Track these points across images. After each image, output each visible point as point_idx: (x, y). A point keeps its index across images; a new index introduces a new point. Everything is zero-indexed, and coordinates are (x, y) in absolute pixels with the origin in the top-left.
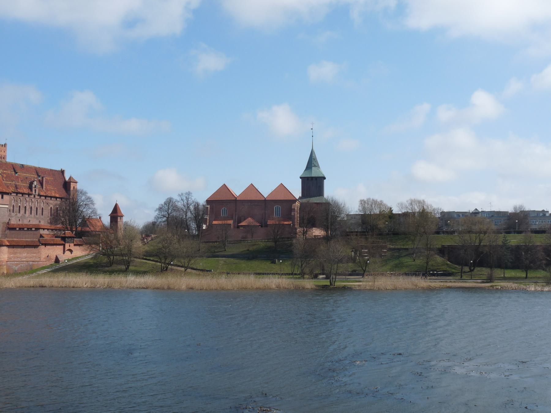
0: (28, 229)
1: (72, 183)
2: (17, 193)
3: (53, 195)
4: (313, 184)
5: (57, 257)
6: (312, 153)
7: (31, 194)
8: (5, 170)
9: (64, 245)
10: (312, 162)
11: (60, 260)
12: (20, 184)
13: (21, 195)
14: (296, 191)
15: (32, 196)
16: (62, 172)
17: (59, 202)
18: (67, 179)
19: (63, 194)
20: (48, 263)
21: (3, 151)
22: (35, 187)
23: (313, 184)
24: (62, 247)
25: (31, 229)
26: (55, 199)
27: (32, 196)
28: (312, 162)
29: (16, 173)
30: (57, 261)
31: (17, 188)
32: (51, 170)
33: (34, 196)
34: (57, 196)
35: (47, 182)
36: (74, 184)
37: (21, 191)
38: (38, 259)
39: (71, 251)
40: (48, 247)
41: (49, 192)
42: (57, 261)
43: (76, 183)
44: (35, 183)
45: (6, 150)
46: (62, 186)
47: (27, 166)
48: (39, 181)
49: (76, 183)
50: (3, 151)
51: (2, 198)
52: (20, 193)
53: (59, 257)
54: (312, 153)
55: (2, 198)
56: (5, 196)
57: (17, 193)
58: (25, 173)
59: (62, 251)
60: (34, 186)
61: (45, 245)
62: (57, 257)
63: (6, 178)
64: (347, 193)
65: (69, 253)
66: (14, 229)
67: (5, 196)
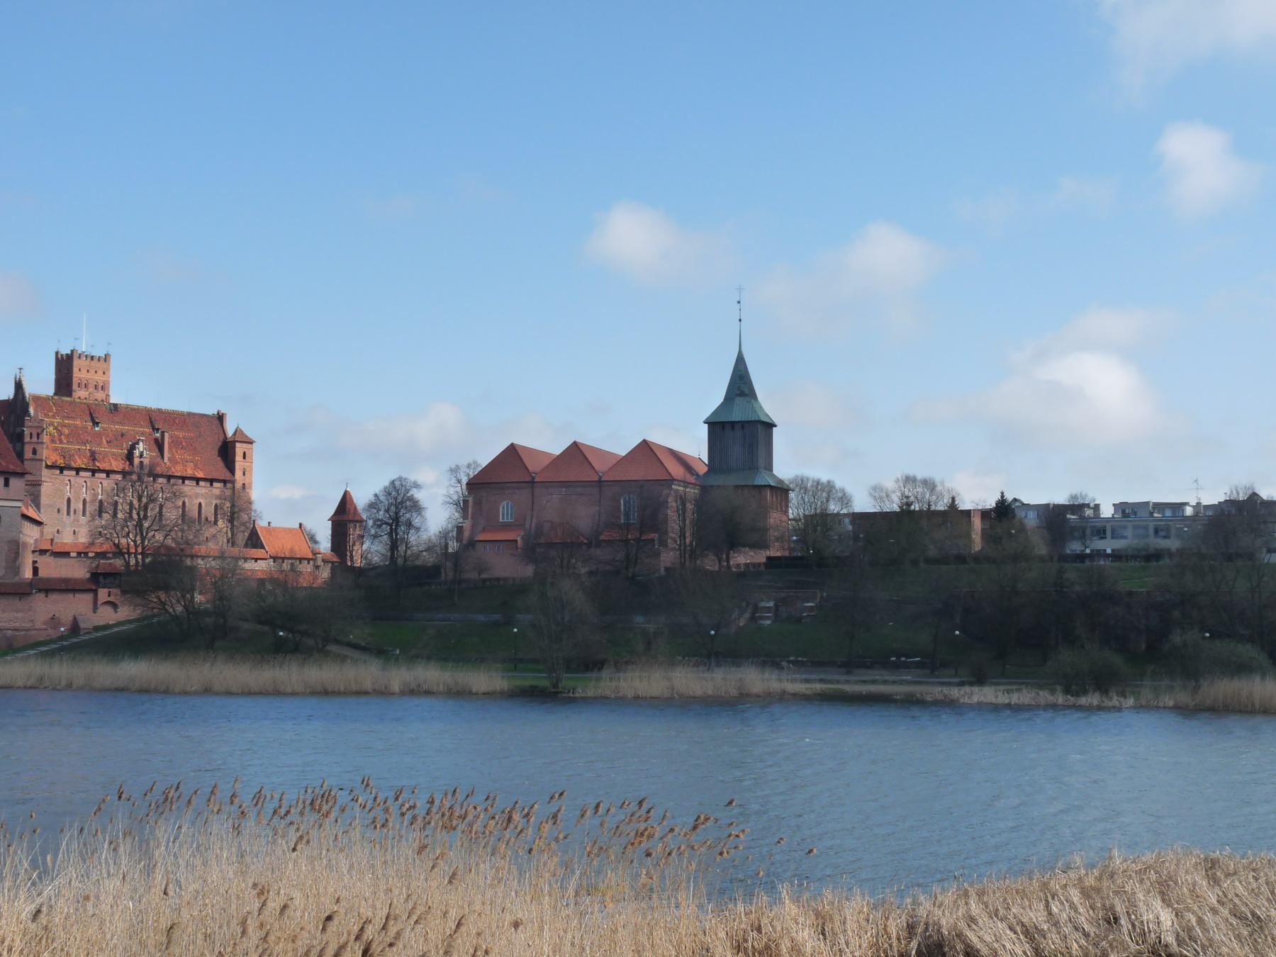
0: (79, 554)
1: (238, 445)
2: (94, 472)
3: (189, 472)
4: (740, 430)
5: (75, 618)
6: (740, 361)
7: (130, 473)
8: (68, 418)
9: (95, 592)
10: (741, 385)
11: (82, 625)
12: (104, 448)
13: (104, 475)
14: (695, 445)
15: (134, 477)
16: (220, 418)
17: (217, 492)
18: (230, 432)
19: (220, 470)
20: (53, 634)
21: (100, 373)
22: (141, 456)
23: (740, 430)
24: (88, 597)
25: (68, 554)
26: (208, 484)
27: (134, 477)
28: (741, 385)
29: (96, 424)
30: (75, 628)
31: (94, 460)
32: (190, 414)
33: (140, 479)
34: (200, 475)
35: (176, 443)
36: (245, 445)
37: (106, 466)
38: (28, 625)
39: (114, 605)
40: (54, 597)
41: (179, 467)
42: (75, 628)
43: (251, 443)
44: (141, 446)
45: (108, 369)
46: (216, 452)
47: (127, 407)
48: (156, 440)
49: (251, 443)
50: (100, 373)
51: (7, 484)
52: (70, 468)
53: (80, 618)
54: (740, 361)
55: (7, 484)
56: (13, 481)
57: (94, 472)
58: (120, 423)
59: (91, 606)
60: (137, 453)
61: (47, 591)
62: (75, 618)
63: (67, 437)
64: (846, 451)
65: (109, 609)
66: (66, 554)
67: (13, 481)
